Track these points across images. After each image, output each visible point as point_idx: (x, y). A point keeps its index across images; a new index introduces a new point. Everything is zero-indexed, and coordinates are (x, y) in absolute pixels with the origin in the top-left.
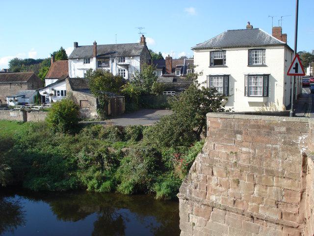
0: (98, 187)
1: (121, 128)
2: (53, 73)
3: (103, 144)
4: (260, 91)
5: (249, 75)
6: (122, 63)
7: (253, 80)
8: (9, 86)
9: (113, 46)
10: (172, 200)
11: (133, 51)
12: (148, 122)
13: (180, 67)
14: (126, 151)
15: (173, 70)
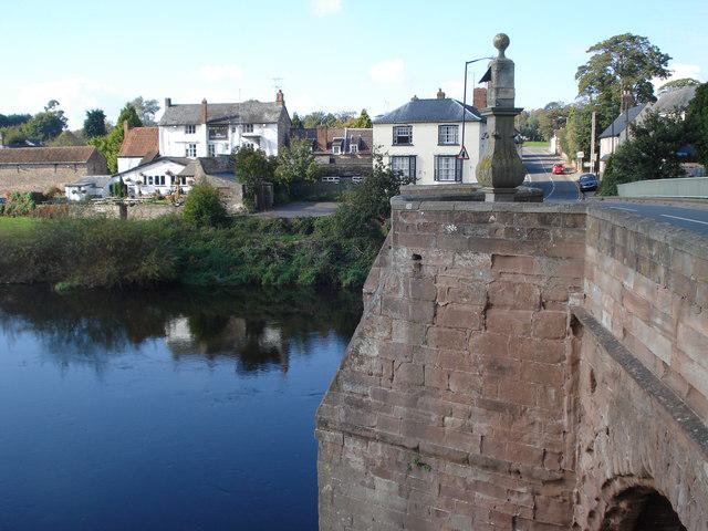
0: (276, 280)
1: (286, 220)
2: (131, 149)
3: (268, 240)
4: (452, 174)
5: (439, 156)
6: (250, 134)
7: (443, 161)
8: (53, 170)
9: (231, 106)
10: (357, 287)
11: (266, 116)
12: (323, 211)
13: (340, 140)
14: (300, 244)
15: (329, 146)
